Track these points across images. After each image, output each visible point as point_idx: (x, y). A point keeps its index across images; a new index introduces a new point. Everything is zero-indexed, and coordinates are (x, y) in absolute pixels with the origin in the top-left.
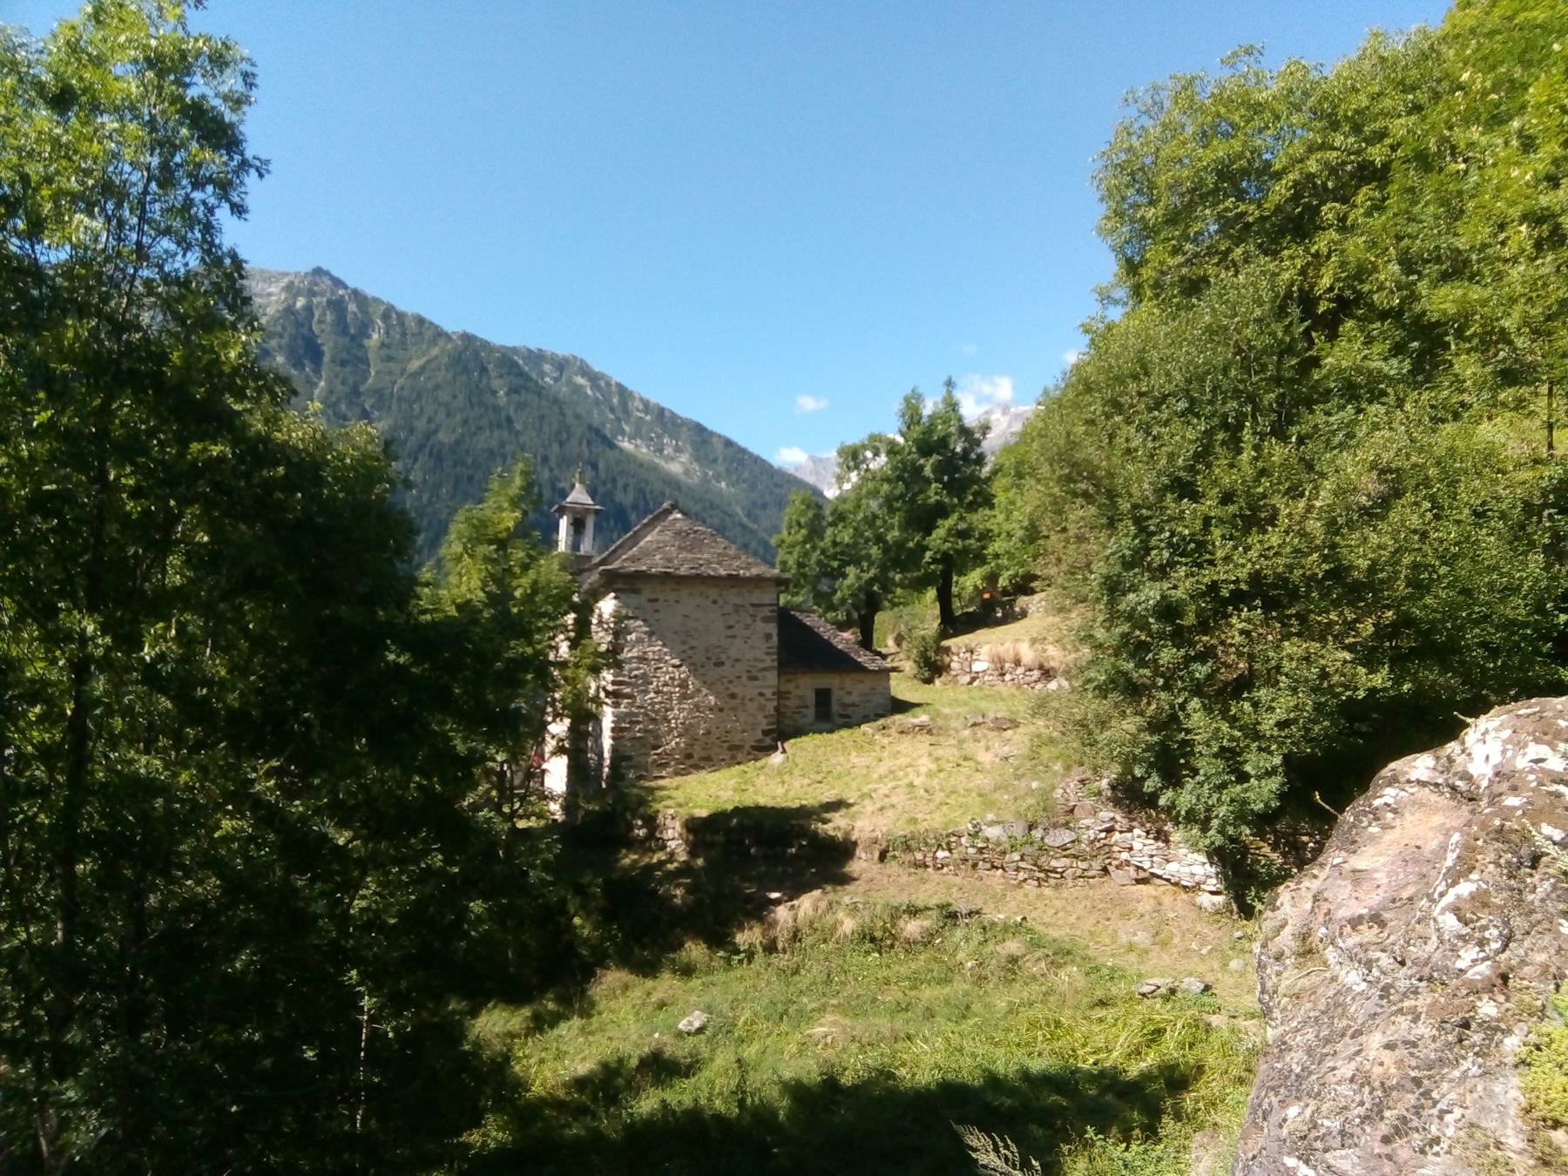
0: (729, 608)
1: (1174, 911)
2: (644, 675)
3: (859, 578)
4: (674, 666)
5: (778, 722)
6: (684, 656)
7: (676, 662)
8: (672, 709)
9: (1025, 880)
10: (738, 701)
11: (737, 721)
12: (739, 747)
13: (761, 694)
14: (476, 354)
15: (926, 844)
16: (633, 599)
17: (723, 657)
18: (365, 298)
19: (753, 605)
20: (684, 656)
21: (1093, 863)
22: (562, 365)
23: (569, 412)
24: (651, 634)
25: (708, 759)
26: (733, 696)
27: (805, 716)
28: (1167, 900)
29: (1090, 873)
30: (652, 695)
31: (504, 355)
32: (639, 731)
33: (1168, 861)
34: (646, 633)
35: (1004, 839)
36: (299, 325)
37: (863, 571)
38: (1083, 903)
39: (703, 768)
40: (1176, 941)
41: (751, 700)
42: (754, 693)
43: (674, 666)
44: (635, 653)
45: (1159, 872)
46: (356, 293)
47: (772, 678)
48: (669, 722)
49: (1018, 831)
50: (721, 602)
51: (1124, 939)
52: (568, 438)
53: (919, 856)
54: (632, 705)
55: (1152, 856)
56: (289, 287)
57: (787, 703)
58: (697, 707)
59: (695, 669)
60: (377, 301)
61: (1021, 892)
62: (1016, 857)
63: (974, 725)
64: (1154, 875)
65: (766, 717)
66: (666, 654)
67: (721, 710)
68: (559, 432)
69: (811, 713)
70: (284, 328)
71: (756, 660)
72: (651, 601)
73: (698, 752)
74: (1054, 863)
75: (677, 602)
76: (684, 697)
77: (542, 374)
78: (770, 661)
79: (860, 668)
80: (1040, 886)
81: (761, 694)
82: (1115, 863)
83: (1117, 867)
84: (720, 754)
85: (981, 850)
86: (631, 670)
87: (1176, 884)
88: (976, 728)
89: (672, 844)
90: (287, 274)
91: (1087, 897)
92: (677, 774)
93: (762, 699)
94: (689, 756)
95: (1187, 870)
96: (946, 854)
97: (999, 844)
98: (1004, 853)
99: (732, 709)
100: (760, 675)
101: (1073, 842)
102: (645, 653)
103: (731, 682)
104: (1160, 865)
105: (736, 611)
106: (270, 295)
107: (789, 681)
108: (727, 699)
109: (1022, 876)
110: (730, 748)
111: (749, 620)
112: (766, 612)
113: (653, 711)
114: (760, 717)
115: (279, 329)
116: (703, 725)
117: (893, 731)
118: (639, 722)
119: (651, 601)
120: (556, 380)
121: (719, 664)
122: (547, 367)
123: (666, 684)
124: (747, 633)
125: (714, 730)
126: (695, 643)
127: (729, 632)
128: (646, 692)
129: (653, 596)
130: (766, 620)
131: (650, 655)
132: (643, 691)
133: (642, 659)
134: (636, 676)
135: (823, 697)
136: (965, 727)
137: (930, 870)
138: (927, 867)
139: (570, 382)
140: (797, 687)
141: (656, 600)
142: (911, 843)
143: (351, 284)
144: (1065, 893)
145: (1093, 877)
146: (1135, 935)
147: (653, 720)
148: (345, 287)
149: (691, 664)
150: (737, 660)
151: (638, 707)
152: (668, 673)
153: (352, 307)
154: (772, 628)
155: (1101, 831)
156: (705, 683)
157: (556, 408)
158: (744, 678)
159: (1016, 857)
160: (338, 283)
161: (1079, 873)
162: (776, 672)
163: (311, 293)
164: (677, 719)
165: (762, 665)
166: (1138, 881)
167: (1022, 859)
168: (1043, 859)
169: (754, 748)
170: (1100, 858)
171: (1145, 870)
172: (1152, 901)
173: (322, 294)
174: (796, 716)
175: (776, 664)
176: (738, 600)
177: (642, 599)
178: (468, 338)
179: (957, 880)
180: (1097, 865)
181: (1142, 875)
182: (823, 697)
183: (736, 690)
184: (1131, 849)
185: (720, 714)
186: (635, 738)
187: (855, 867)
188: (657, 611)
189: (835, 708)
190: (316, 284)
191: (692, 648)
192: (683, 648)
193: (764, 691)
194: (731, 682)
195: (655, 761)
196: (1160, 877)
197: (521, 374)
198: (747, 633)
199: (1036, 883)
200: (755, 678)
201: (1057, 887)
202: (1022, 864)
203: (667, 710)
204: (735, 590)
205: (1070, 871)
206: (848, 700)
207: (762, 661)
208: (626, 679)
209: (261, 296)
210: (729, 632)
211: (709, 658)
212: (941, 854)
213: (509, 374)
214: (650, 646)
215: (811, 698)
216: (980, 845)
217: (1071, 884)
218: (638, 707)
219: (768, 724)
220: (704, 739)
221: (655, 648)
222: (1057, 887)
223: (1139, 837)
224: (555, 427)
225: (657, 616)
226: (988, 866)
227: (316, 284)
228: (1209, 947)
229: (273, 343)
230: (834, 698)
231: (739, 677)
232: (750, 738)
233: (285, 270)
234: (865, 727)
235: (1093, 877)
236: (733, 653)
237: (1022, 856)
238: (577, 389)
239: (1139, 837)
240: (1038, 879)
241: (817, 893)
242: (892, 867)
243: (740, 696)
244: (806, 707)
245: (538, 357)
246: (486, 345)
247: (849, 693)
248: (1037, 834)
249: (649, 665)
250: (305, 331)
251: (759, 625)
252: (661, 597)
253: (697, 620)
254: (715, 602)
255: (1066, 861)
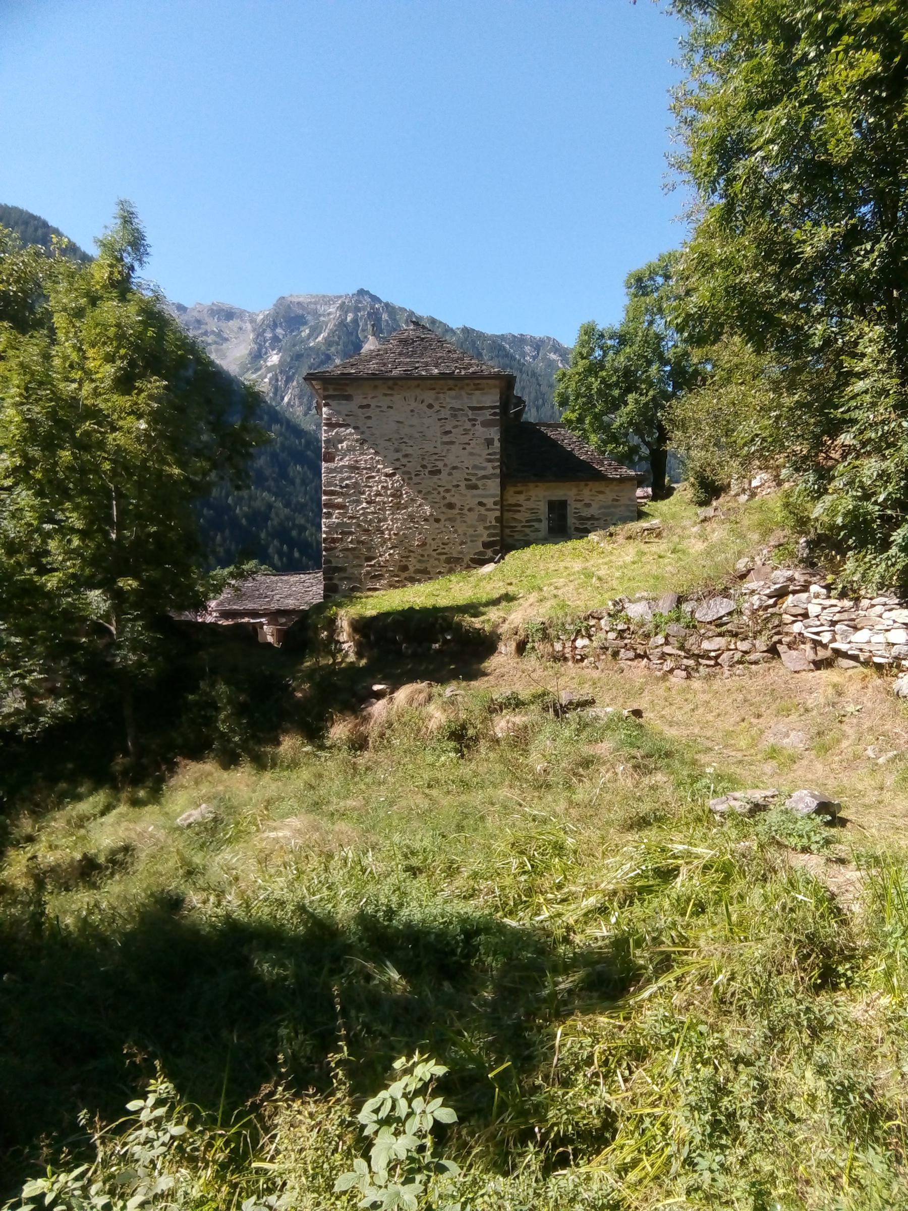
0: (445, 413)
1: (857, 703)
2: (356, 484)
3: (637, 402)
4: (387, 475)
5: (502, 534)
6: (398, 464)
7: (389, 470)
8: (385, 520)
9: (671, 671)
10: (457, 511)
11: (456, 532)
12: (458, 560)
13: (481, 504)
14: (473, 343)
15: (565, 631)
16: (345, 407)
17: (440, 465)
18: (394, 308)
19: (473, 408)
20: (398, 464)
21: (757, 642)
22: (538, 345)
23: (544, 383)
24: (363, 442)
25: (425, 572)
26: (451, 506)
27: (537, 530)
28: (853, 689)
29: (752, 657)
30: (364, 505)
31: (494, 342)
32: (351, 542)
33: (856, 628)
34: (357, 441)
35: (649, 618)
36: (349, 334)
37: (641, 395)
38: (734, 696)
39: (419, 581)
40: (845, 744)
41: (470, 510)
42: (473, 502)
43: (387, 475)
44: (346, 462)
45: (843, 647)
46: (387, 305)
47: (494, 486)
48: (383, 533)
49: (665, 606)
50: (437, 407)
51: (769, 740)
52: (544, 404)
53: (558, 647)
54: (343, 515)
55: (833, 623)
56: (342, 307)
57: (518, 516)
58: (411, 518)
59: (408, 478)
60: (403, 310)
61: (663, 685)
62: (660, 639)
63: (705, 520)
64: (838, 653)
65: (486, 528)
66: (378, 462)
67: (437, 520)
68: (536, 399)
69: (544, 526)
70: (339, 338)
71: (475, 467)
72: (361, 407)
73: (413, 565)
74: (706, 645)
75: (389, 407)
76: (398, 507)
77: (524, 355)
78: (492, 468)
79: (599, 477)
80: (689, 677)
81: (481, 504)
82: (786, 639)
83: (790, 646)
84: (437, 567)
85: (621, 634)
86: (342, 480)
87: (866, 663)
88: (706, 524)
89: (345, 646)
90: (341, 297)
91: (740, 690)
92: (392, 586)
93: (482, 509)
94: (405, 568)
95: (880, 638)
96: (586, 641)
97: (642, 625)
98: (647, 636)
99: (450, 519)
100: (480, 483)
101: (730, 614)
102: (357, 461)
103: (447, 491)
104: (845, 635)
105: (455, 416)
106: (329, 314)
107: (520, 493)
108: (444, 509)
109: (669, 664)
110: (448, 561)
111: (468, 425)
112: (487, 415)
113: (365, 521)
114: (480, 530)
115: (336, 338)
116: (418, 537)
117: (620, 539)
118: (351, 533)
119: (361, 407)
120: (534, 358)
121: (435, 472)
122: (527, 349)
123: (378, 494)
124: (466, 439)
125: (429, 541)
126: (410, 451)
127: (446, 439)
128: (358, 502)
129: (365, 402)
130: (486, 424)
131: (362, 464)
132: (354, 501)
133: (354, 468)
134: (347, 486)
135: (558, 509)
136: (695, 523)
137: (570, 663)
138: (566, 659)
139: (545, 359)
140: (528, 500)
141: (368, 406)
142: (550, 631)
143: (384, 299)
144: (717, 684)
145: (756, 663)
146: (787, 735)
147: (366, 531)
148: (380, 301)
149: (404, 473)
150: (455, 468)
151: (350, 518)
152: (380, 482)
153: (385, 316)
154: (494, 433)
155: (770, 597)
156: (420, 492)
157: (534, 380)
158: (463, 487)
159: (660, 639)
160: (375, 299)
161: (738, 656)
162: (499, 480)
163: (357, 309)
164: (392, 529)
165: (481, 473)
166: (818, 665)
167: (667, 643)
168: (692, 640)
169: (472, 560)
170: (766, 633)
171: (825, 646)
172: (830, 690)
173: (364, 309)
174: (527, 530)
175: (498, 471)
176: (456, 404)
177: (353, 406)
178: (466, 331)
179: (596, 674)
180: (761, 643)
181: (822, 654)
182: (558, 509)
183: (453, 500)
184: (806, 616)
185: (437, 525)
186: (347, 550)
187: (493, 663)
188: (369, 418)
189: (571, 521)
190: (360, 302)
191: (406, 456)
192: (397, 455)
193: (484, 501)
194: (447, 491)
195: (368, 573)
196: (845, 655)
197: (507, 355)
198: (466, 439)
199: (684, 674)
200: (475, 487)
201: (709, 678)
202: (668, 649)
203: (380, 521)
204: (453, 393)
205: (726, 655)
206: (586, 513)
207: (484, 468)
208: (338, 489)
209: (324, 316)
210: (446, 439)
211: (424, 467)
212: (580, 643)
213: (498, 356)
214: (362, 454)
215: (543, 508)
216: (620, 627)
217: (727, 673)
218: (350, 518)
219: (489, 536)
220: (420, 551)
221: (366, 458)
222: (709, 678)
223: (817, 596)
224: (533, 395)
225: (369, 423)
226: (631, 654)
227: (360, 302)
228: (891, 754)
229: (333, 349)
230: (570, 510)
231: (458, 486)
232: (470, 550)
233: (331, 293)
234: (593, 537)
235: (756, 663)
236: (451, 460)
237: (666, 638)
238: (551, 364)
239: (817, 596)
240: (686, 669)
241: (422, 685)
242: (531, 662)
243: (458, 505)
244: (540, 521)
245: (520, 341)
246: (481, 336)
247: (588, 505)
248: (686, 607)
249: (361, 475)
250: (353, 338)
251: (480, 430)
252: (373, 403)
253: (412, 426)
254: (430, 406)
255: (720, 642)
